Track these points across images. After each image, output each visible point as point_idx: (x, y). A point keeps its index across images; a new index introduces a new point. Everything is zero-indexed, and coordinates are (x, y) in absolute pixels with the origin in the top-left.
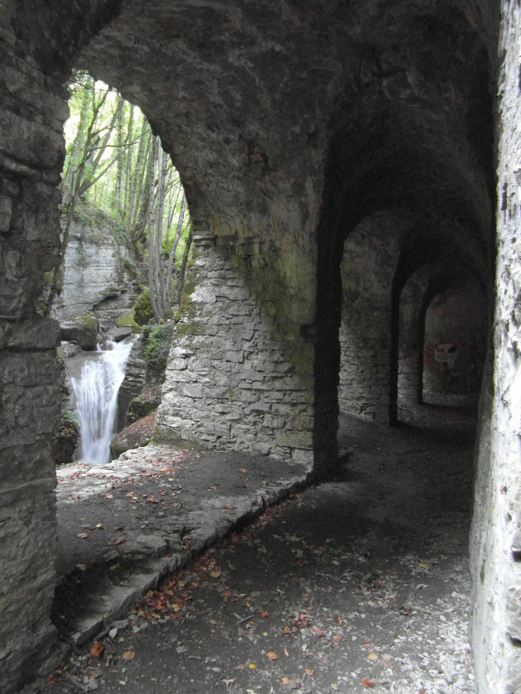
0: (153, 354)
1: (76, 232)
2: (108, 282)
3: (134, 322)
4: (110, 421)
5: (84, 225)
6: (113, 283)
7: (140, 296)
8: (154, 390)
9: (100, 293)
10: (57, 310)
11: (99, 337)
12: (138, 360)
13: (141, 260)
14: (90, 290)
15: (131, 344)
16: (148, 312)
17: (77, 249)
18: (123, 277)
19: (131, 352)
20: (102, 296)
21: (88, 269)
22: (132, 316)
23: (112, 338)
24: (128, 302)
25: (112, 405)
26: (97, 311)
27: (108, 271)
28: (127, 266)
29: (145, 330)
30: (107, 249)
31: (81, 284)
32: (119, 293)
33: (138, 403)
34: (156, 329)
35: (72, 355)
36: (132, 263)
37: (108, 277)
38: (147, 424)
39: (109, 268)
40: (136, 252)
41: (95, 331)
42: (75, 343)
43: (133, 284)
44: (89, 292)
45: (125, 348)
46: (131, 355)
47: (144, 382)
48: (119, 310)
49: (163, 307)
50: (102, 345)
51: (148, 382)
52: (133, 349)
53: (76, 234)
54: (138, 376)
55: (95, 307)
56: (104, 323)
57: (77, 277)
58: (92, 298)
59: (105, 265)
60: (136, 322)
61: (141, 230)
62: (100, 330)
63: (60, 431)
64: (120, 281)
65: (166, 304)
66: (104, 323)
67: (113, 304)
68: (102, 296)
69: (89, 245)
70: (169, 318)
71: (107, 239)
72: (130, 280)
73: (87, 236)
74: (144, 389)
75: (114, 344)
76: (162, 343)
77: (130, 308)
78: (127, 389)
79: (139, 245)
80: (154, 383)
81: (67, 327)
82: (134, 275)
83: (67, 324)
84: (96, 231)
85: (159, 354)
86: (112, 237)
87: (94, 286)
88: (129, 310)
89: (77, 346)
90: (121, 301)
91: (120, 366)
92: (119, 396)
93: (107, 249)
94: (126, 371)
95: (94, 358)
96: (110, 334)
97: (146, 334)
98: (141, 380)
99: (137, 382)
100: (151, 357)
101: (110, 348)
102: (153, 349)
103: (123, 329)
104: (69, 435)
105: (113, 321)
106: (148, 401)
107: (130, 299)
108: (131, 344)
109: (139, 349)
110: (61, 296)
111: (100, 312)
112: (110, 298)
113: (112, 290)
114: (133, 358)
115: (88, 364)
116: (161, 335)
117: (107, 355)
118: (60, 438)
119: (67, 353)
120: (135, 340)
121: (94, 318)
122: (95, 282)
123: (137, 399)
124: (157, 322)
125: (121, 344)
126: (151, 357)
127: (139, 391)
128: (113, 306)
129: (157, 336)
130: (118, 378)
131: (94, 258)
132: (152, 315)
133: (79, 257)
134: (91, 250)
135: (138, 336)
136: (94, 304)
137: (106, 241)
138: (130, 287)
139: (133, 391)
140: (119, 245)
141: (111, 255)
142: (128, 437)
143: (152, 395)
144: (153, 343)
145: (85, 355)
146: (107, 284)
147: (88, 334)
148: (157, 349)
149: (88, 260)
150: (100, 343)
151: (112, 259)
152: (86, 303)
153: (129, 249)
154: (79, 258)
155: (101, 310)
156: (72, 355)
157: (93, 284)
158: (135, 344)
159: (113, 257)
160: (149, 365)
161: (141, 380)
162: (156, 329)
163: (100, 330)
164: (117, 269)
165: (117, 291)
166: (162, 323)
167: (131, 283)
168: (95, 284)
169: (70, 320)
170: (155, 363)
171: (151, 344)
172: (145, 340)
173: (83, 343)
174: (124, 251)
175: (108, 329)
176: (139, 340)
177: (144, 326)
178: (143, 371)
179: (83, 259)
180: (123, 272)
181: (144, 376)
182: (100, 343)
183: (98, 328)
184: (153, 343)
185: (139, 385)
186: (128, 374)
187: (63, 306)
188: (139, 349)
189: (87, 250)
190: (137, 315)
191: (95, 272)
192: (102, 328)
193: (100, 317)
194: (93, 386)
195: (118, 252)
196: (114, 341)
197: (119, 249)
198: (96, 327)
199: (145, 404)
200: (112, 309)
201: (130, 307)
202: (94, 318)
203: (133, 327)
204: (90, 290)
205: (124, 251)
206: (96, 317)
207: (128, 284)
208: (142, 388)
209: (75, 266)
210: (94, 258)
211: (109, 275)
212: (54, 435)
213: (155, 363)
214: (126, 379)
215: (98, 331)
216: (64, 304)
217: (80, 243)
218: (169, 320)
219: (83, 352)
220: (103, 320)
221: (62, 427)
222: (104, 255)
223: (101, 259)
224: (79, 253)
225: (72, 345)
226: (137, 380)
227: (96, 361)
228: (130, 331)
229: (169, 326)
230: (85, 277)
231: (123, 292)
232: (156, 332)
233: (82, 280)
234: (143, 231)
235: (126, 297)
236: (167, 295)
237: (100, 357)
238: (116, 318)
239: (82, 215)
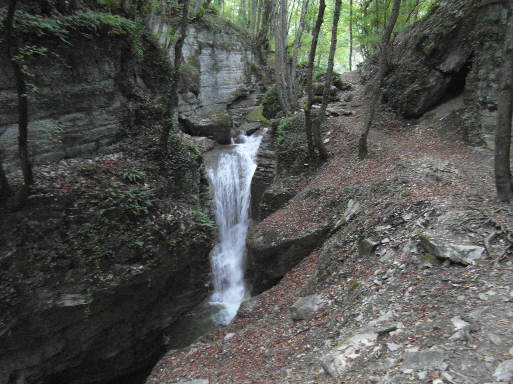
0: (283, 145)
1: (209, 40)
2: (238, 84)
3: (262, 116)
4: (245, 205)
5: (215, 33)
6: (242, 85)
7: (266, 94)
8: (285, 181)
9: (232, 94)
10: (196, 111)
11: (233, 131)
12: (268, 152)
13: (265, 64)
14: (224, 91)
15: (261, 137)
16: (275, 106)
17: (210, 55)
18: (250, 79)
19: (261, 144)
20: (234, 96)
21: (221, 72)
22: (260, 112)
23: (243, 132)
24: (256, 100)
25: (246, 192)
26: (230, 110)
27: (238, 74)
28: (254, 69)
29: (274, 123)
30: (236, 54)
31: (215, 87)
32: (248, 93)
33: (271, 195)
34: (284, 121)
35: (210, 149)
36: (257, 66)
37: (238, 79)
38: (282, 220)
39: (238, 71)
40: (261, 57)
41: (229, 127)
42: (211, 138)
43: (260, 85)
44: (223, 93)
45: (256, 140)
46: (261, 147)
47: (275, 172)
48: (249, 108)
49: (290, 100)
50: (236, 139)
51: (279, 173)
52: (263, 141)
53: (208, 42)
54: (268, 166)
55: (229, 107)
56: (236, 120)
57: (212, 80)
58: (225, 98)
59: (235, 69)
60: (265, 117)
61: (264, 35)
62: (234, 126)
63: (192, 237)
64: (248, 83)
65: (292, 97)
66: (236, 120)
67: (243, 103)
68: (234, 96)
69: (220, 51)
70: (297, 110)
71: (235, 45)
72: (257, 82)
73: (218, 43)
74: (275, 179)
75: (246, 137)
76: (291, 135)
77: (258, 105)
78: (259, 179)
79: (263, 51)
80: (285, 174)
81: (205, 124)
82: (259, 77)
83: (204, 122)
84: (226, 37)
85: (289, 145)
86: (240, 44)
87: (227, 88)
88: (257, 107)
89: (214, 141)
90: (249, 100)
91: (252, 157)
92: (253, 186)
93: (236, 54)
94: (258, 161)
95: (229, 151)
96: (242, 129)
97: (275, 127)
98: (272, 170)
99: (268, 172)
100: (281, 149)
101: (242, 142)
102: (283, 141)
103: (253, 124)
104: (202, 241)
105: (244, 117)
106: (280, 193)
107: (257, 98)
108: (261, 137)
109: (269, 141)
110: (199, 97)
111: (233, 111)
112: (241, 97)
113: (243, 90)
114: (263, 150)
115: (224, 156)
116: (290, 126)
117: (241, 149)
118: (191, 245)
119: (206, 148)
120: (264, 133)
121: (227, 114)
122: (227, 84)
123: (270, 191)
124: (285, 114)
125: (252, 138)
126: (281, 149)
127: (270, 180)
128: (243, 105)
129: (285, 129)
130: (251, 168)
131: (225, 62)
132: (279, 109)
133: (212, 62)
134: (222, 55)
135: (266, 129)
136: (229, 103)
137: (234, 48)
138: (257, 88)
139: (264, 180)
140: (246, 50)
141: (239, 59)
142: (263, 234)
143: (284, 187)
144: (282, 135)
145: (221, 149)
146: (237, 85)
147: (223, 130)
148: (287, 140)
149: (220, 64)
150: (234, 137)
151: (241, 63)
152: (221, 103)
153: (255, 54)
154: (212, 63)
155: (234, 108)
156: (210, 149)
157: (226, 86)
158: (264, 137)
159: (241, 61)
160: (279, 157)
161: (272, 170)
162: (284, 121)
163: (234, 126)
164: (246, 72)
165: (246, 91)
166: (289, 116)
167: (257, 84)
168: (228, 86)
169: (207, 117)
170: (285, 155)
171: (280, 136)
172: (274, 133)
173: (219, 137)
174: (251, 56)
175: (240, 124)
176: (267, 133)
177: (272, 119)
178: (273, 162)
179: (216, 64)
180: (251, 74)
181: (275, 166)
182: (234, 137)
183: (232, 124)
184: (282, 135)
185: (270, 175)
186: (260, 165)
187: (201, 107)
188: (269, 141)
189: (219, 56)
190: (265, 110)
191: (226, 75)
192: (235, 124)
193: (233, 115)
194: (229, 175)
195: (246, 57)
196: (245, 135)
197: (246, 54)
198: (229, 123)
199: (277, 196)
200: (243, 107)
201: (257, 105)
202: (227, 114)
203: (261, 122)
204: (224, 91)
205: (250, 56)
206: (229, 114)
207: (255, 85)
208: (273, 178)
209: (209, 70)
210: (225, 62)
211: (239, 77)
212: (184, 244)
213: (285, 154)
214: (257, 169)
215: (232, 127)
216: (202, 104)
217: (213, 50)
218: (296, 112)
219: (220, 146)
220: (235, 117)
221: (193, 232)
222: (233, 59)
223: (231, 63)
224: (213, 59)
225: (209, 140)
226: (268, 170)
227: (230, 154)
228: (259, 125)
229: (297, 118)
230: (218, 80)
231: (252, 92)
232: (285, 124)
233: (216, 82)
234: (265, 37)
235: (254, 97)
236: (293, 88)
237: (234, 150)
238: (247, 114)
239: (213, 23)
